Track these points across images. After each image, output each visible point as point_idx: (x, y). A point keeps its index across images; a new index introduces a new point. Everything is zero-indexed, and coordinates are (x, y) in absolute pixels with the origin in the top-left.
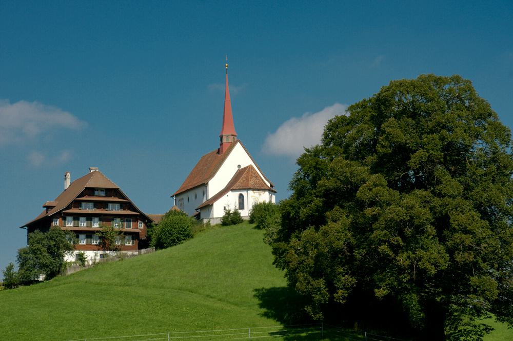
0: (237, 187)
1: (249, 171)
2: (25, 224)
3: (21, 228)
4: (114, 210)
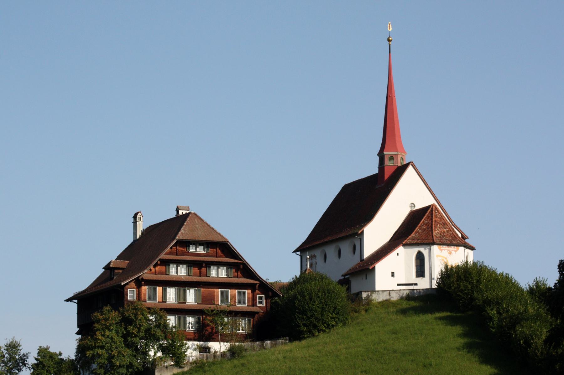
0: (413, 240)
1: (432, 214)
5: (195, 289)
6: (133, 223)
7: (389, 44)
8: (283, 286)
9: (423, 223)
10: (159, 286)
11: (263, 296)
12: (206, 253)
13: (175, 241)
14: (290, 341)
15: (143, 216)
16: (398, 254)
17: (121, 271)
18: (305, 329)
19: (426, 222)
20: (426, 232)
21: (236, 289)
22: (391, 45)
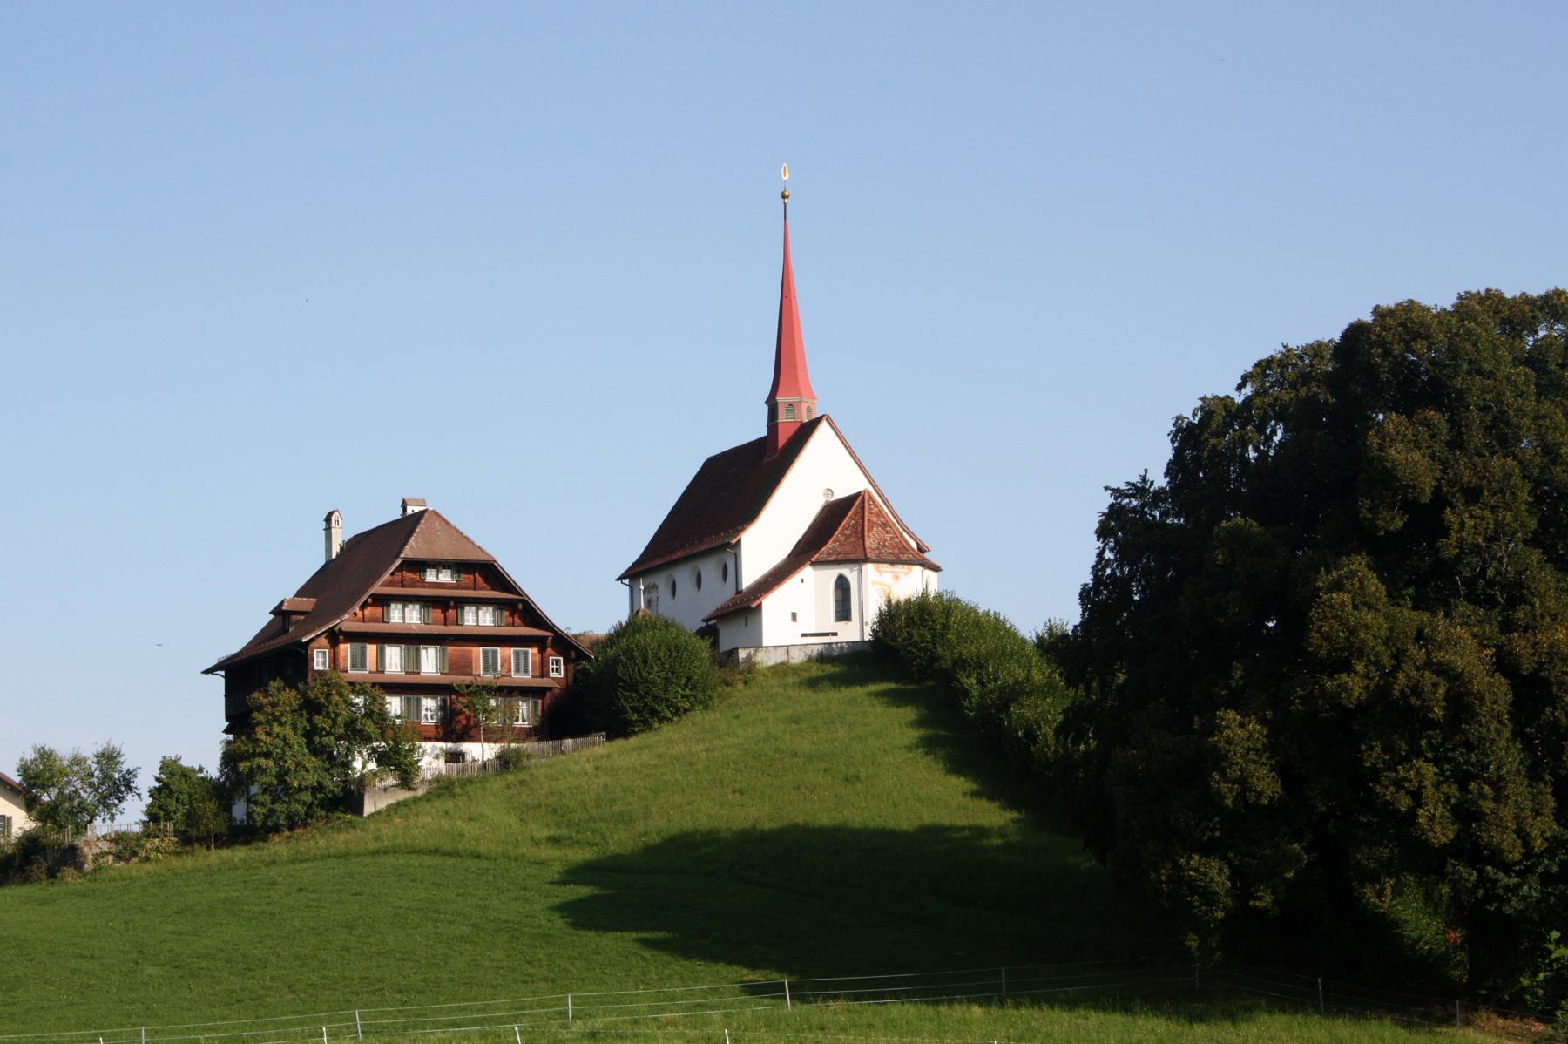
0: (829, 554)
2: (214, 662)
3: (206, 672)
4: (480, 619)
7: (785, 204)
8: (598, 640)
9: (848, 523)
10: (370, 643)
13: (398, 562)
16: (802, 581)
17: (302, 617)
18: (635, 717)
20: (853, 539)
21: (511, 647)
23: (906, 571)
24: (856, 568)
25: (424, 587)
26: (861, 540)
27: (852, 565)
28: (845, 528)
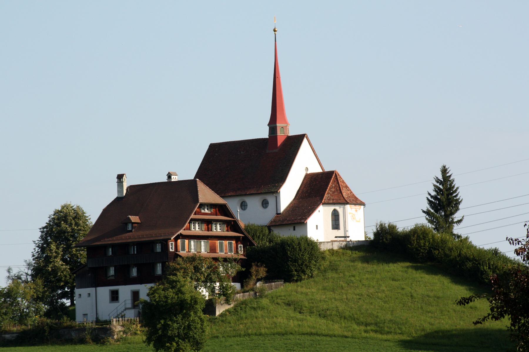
5: (195, 241)
6: (117, 183)
7: (275, 34)
9: (332, 186)
10: (186, 239)
11: (241, 246)
12: (210, 212)
13: (199, 204)
14: (285, 282)
15: (127, 177)
17: (136, 225)
18: (296, 273)
19: (334, 185)
20: (336, 193)
21: (227, 240)
22: (276, 35)
23: (359, 208)
24: (342, 206)
25: (201, 215)
26: (340, 194)
27: (340, 205)
28: (330, 188)
